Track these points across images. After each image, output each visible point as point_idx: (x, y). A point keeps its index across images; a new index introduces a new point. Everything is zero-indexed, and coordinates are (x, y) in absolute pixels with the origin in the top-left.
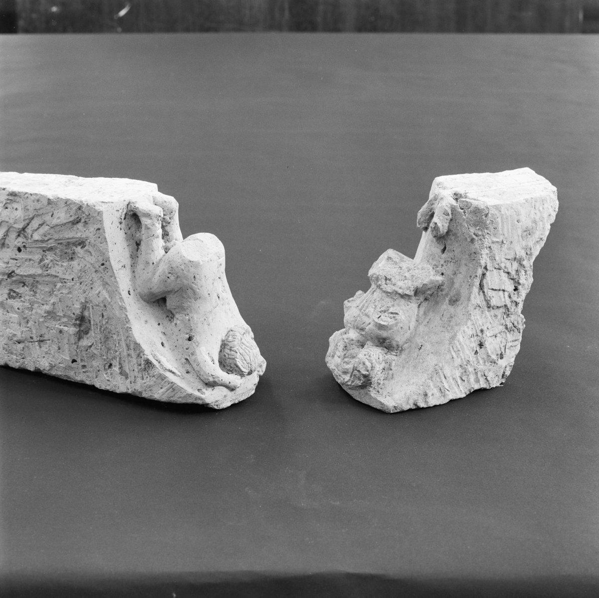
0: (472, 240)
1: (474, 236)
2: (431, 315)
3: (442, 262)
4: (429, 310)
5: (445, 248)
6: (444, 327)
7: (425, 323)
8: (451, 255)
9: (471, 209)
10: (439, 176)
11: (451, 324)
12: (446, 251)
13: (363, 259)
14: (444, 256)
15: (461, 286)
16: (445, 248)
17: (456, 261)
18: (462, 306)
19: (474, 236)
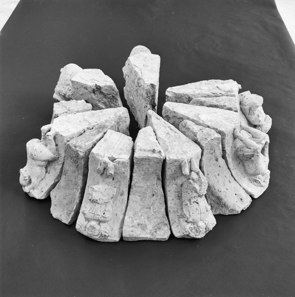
0: (124, 173)
1: (124, 171)
2: (115, 202)
3: (114, 183)
4: (114, 201)
5: (113, 178)
6: (121, 204)
7: (114, 206)
8: (117, 180)
9: (121, 163)
10: (60, 70)
11: (124, 202)
12: (114, 179)
13: (156, 189)
14: (114, 181)
15: (145, 222)
16: (113, 178)
17: (119, 181)
18: (94, 81)
19: (124, 171)
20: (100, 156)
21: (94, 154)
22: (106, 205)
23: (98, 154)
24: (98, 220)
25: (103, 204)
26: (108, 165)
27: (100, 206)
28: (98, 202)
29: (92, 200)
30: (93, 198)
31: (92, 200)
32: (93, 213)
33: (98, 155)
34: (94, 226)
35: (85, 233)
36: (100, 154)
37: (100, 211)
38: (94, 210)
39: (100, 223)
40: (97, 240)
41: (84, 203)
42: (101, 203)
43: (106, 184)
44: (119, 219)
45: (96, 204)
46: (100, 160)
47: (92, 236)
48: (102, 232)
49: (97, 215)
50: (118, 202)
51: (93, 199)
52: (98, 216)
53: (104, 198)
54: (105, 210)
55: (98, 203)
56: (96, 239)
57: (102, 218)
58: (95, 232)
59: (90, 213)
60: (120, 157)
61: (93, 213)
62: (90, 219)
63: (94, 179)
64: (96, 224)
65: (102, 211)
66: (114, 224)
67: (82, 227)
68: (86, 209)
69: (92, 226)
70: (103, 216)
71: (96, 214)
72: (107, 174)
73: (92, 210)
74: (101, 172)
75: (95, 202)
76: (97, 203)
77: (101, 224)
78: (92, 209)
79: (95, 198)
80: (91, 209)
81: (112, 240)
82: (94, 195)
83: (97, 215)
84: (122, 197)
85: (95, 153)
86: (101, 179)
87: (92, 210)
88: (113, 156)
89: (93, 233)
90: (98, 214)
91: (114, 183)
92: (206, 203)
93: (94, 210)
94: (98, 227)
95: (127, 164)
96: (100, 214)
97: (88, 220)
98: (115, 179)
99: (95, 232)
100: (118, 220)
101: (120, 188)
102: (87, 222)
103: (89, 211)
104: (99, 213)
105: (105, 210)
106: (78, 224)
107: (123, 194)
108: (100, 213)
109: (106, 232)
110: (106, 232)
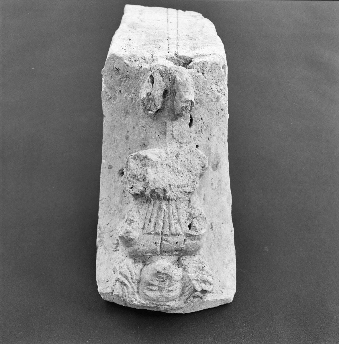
5: (192, 120)
9: (209, 67)
16: (192, 120)
20: (141, 60)
21: (120, 59)
22: (189, 201)
23: (134, 56)
24: (176, 250)
25: (181, 199)
26: (175, 77)
27: (174, 206)
28: (168, 194)
29: (148, 192)
30: (152, 186)
31: (148, 192)
32: (158, 234)
33: (133, 59)
34: (166, 272)
35: (137, 300)
36: (139, 55)
37: (179, 221)
38: (160, 222)
39: (181, 260)
40: (177, 312)
41: (106, 216)
42: (175, 198)
43: (174, 141)
44: (219, 237)
45: (164, 203)
46: (145, 71)
47: (161, 303)
48: (194, 282)
49: (173, 235)
50: (209, 188)
51: (153, 188)
52: (172, 239)
53: (181, 182)
54: (192, 216)
55: (169, 200)
56: (172, 309)
57: (188, 242)
58: (171, 288)
59: (150, 233)
60: (200, 52)
61: (158, 234)
62: (151, 254)
63: (127, 138)
64: (169, 264)
65: (183, 221)
66: (211, 254)
67: (127, 283)
68: (133, 225)
69: (163, 272)
70: (190, 235)
71: (168, 233)
72: (173, 109)
73: (152, 224)
74: (157, 104)
75: (158, 197)
76: (165, 198)
77: (186, 261)
78: (153, 220)
79: (157, 186)
80: (148, 221)
81: (216, 301)
82: (151, 175)
83: (173, 235)
84: (217, 174)
85: (122, 56)
86: (154, 131)
87: (152, 224)
88: (180, 54)
89: (165, 294)
90: (173, 231)
91: (193, 135)
92: (99, 267)
93: (160, 222)
94: (177, 273)
95: (223, 70)
96: (179, 231)
97: (141, 257)
98: (196, 121)
99: (169, 289)
100: (219, 239)
101: (209, 149)
102: (140, 265)
103: (144, 228)
104: (176, 227)
105: (192, 216)
106: (103, 279)
107: (218, 163)
108: (178, 227)
109: (204, 281)
110: (204, 281)
